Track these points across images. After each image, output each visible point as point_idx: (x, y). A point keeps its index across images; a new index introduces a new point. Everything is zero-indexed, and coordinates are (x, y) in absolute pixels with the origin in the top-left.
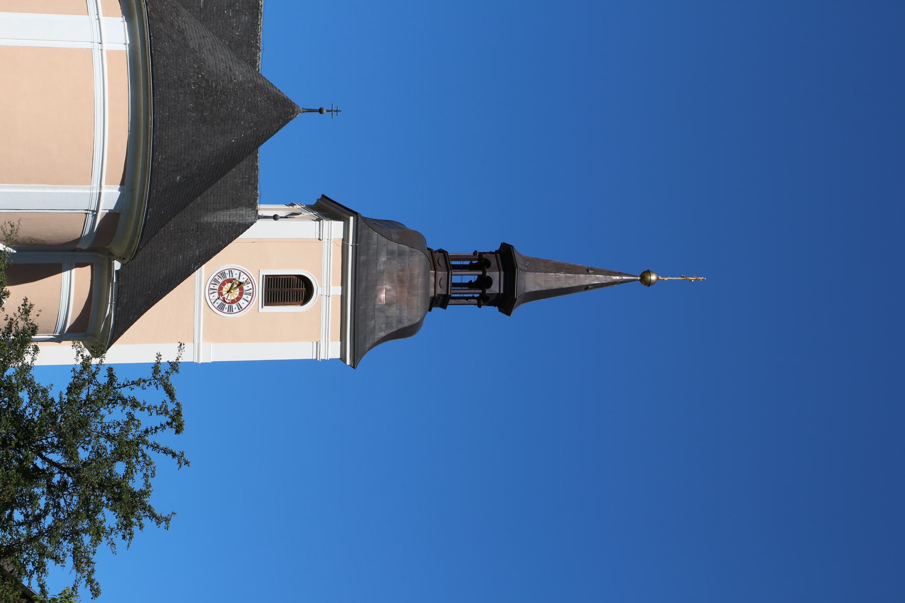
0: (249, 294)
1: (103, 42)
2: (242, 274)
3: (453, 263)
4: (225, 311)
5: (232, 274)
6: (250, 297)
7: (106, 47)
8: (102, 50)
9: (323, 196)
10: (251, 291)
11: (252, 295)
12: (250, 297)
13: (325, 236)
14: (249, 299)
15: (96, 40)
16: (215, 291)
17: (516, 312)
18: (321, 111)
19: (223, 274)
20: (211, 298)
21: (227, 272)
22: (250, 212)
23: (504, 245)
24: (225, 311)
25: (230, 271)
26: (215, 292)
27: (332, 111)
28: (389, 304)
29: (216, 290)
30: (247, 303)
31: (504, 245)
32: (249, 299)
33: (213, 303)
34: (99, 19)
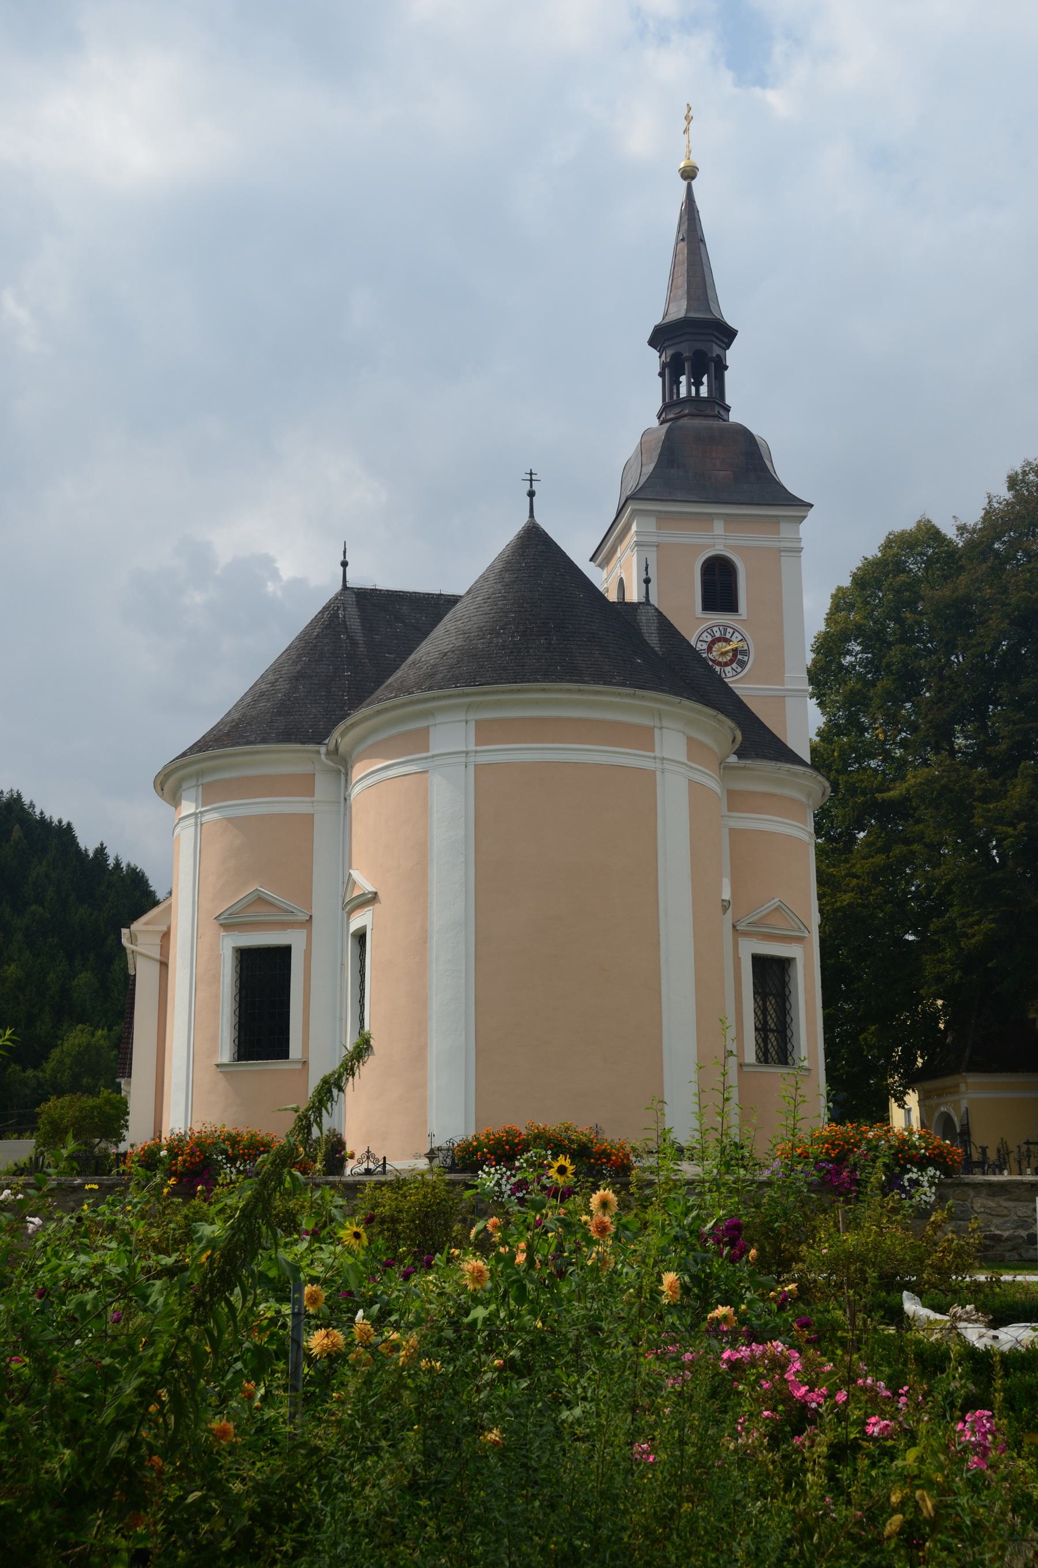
0: (725, 630)
1: (464, 749)
3: (675, 397)
4: (746, 658)
6: (729, 630)
7: (472, 747)
8: (476, 752)
9: (591, 560)
11: (726, 627)
12: (729, 630)
13: (654, 539)
14: (731, 631)
15: (463, 759)
17: (730, 319)
18: (531, 494)
20: (730, 675)
22: (642, 610)
23: (653, 342)
24: (746, 658)
27: (531, 480)
28: (77, 1346)
30: (736, 634)
31: (653, 342)
32: (731, 631)
33: (738, 673)
34: (433, 756)
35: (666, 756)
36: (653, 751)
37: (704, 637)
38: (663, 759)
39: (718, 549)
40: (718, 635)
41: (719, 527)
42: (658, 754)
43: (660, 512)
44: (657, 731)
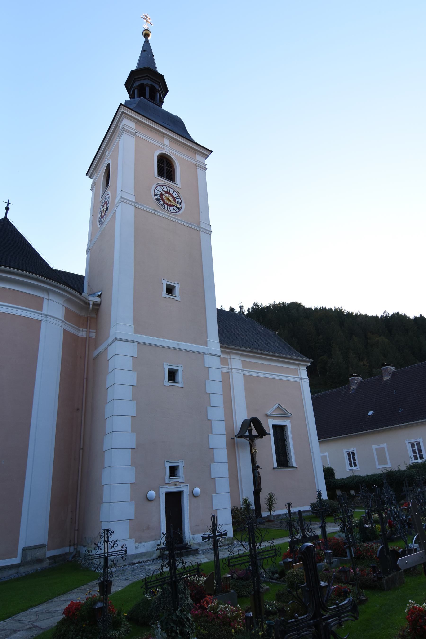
19: (157, 200)
38: (231, 368)
41: (167, 142)
42: (230, 367)
43: (138, 121)
44: (229, 360)
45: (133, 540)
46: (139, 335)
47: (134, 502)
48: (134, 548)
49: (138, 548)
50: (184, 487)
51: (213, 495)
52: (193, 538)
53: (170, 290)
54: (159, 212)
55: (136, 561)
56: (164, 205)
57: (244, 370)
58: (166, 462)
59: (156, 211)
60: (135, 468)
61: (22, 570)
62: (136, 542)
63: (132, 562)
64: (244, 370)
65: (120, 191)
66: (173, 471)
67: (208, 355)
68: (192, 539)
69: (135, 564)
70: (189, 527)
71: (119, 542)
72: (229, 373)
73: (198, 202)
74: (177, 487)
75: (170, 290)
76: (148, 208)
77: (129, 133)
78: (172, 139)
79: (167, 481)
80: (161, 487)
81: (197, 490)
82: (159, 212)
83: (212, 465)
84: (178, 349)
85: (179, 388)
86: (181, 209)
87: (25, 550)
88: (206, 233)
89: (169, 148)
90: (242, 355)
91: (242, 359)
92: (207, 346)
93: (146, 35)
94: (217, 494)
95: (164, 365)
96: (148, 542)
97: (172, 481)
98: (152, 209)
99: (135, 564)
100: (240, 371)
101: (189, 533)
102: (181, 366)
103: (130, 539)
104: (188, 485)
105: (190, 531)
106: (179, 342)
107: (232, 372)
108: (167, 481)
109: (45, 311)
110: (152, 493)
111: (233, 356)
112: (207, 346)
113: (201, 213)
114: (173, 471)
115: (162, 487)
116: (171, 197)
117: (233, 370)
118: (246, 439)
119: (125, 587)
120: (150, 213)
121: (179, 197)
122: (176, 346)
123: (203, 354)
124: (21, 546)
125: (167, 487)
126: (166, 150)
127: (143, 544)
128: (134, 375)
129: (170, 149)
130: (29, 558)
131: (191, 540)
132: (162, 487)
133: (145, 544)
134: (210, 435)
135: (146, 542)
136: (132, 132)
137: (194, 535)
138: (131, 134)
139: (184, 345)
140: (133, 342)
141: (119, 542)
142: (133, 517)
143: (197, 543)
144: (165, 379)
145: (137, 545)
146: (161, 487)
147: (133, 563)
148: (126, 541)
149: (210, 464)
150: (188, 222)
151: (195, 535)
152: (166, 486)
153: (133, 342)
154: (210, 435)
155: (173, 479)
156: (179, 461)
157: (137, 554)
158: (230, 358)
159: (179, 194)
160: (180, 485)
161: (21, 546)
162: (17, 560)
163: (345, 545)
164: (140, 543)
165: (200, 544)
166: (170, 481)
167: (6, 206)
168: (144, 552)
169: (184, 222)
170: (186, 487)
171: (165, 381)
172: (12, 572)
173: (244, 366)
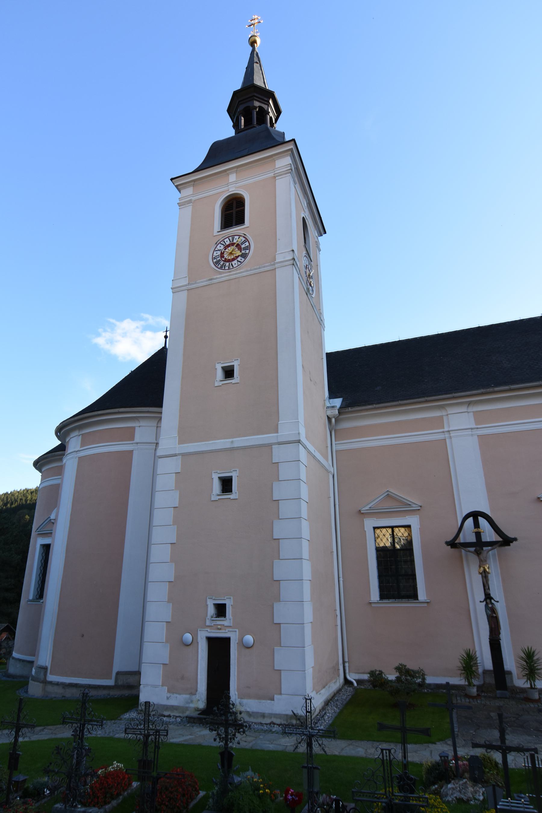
2: (216, 249)
5: (217, 256)
10: (230, 238)
11: (233, 237)
16: (230, 264)
19: (216, 263)
21: (215, 261)
24: (247, 251)
25: (213, 258)
26: (232, 264)
29: (229, 264)
35: (451, 429)
36: (443, 428)
37: (218, 248)
38: (449, 431)
39: (233, 190)
40: (228, 243)
42: (446, 429)
43: (194, 181)
44: (445, 418)
45: (166, 688)
46: (184, 445)
47: (168, 645)
48: (166, 698)
49: (170, 698)
50: (232, 632)
51: (275, 648)
52: (240, 703)
53: (229, 373)
54: (216, 278)
55: (166, 713)
56: (230, 264)
57: (477, 428)
58: (208, 598)
59: (211, 279)
60: (171, 604)
61: (113, 693)
62: (169, 691)
63: (162, 713)
64: (477, 428)
65: (172, 281)
66: (221, 610)
67: (279, 444)
68: (239, 704)
69: (165, 716)
70: (236, 687)
71: (151, 687)
72: (445, 439)
73: (276, 229)
74: (221, 631)
75: (229, 373)
76: (202, 282)
77: (185, 205)
78: (238, 169)
79: (208, 623)
80: (200, 630)
81: (249, 639)
82: (216, 278)
83: (276, 606)
84: (232, 449)
85: (232, 500)
86: (215, 265)
87: (118, 673)
88: (286, 266)
89: (234, 184)
90: (469, 404)
91: (473, 410)
92: (277, 432)
93: (253, 43)
94: (282, 647)
95: (213, 474)
96: (182, 695)
97: (214, 623)
98: (207, 281)
99: (165, 716)
100: (469, 432)
101: (235, 694)
102: (236, 471)
103: (162, 686)
104: (237, 630)
105: (237, 693)
106: (234, 439)
107: (451, 438)
108: (208, 623)
109: (137, 439)
110: (188, 637)
111: (450, 410)
112: (277, 432)
113: (278, 242)
114: (221, 610)
115: (201, 629)
116: (229, 248)
117: (452, 434)
118: (464, 549)
119: (327, 739)
120: (206, 285)
121: (247, 240)
122: (228, 446)
123: (270, 446)
124: (115, 670)
125: (207, 631)
126: (230, 190)
127: (175, 695)
128: (177, 494)
129: (236, 184)
130: (120, 683)
131: (237, 706)
132: (201, 629)
133: (177, 695)
134: (276, 561)
135: (180, 694)
136: (187, 201)
137: (242, 698)
138: (187, 204)
139: (240, 442)
140: (175, 455)
141: (151, 687)
142: (167, 662)
143: (246, 711)
144: (212, 492)
145: (169, 695)
146: (200, 630)
147: (163, 715)
148: (157, 687)
149: (273, 604)
150: (255, 267)
151: (243, 700)
152: (206, 629)
153: (175, 455)
154: (276, 561)
155: (215, 621)
156: (225, 598)
157: (168, 705)
158: (447, 415)
159: (246, 236)
160: (226, 630)
161: (115, 670)
162: (111, 682)
163: (329, 797)
164: (173, 693)
165: (251, 713)
166: (211, 624)
167: (165, 334)
168: (176, 706)
169: (251, 270)
170: (234, 633)
171: (212, 495)
172: (105, 692)
173: (477, 422)
